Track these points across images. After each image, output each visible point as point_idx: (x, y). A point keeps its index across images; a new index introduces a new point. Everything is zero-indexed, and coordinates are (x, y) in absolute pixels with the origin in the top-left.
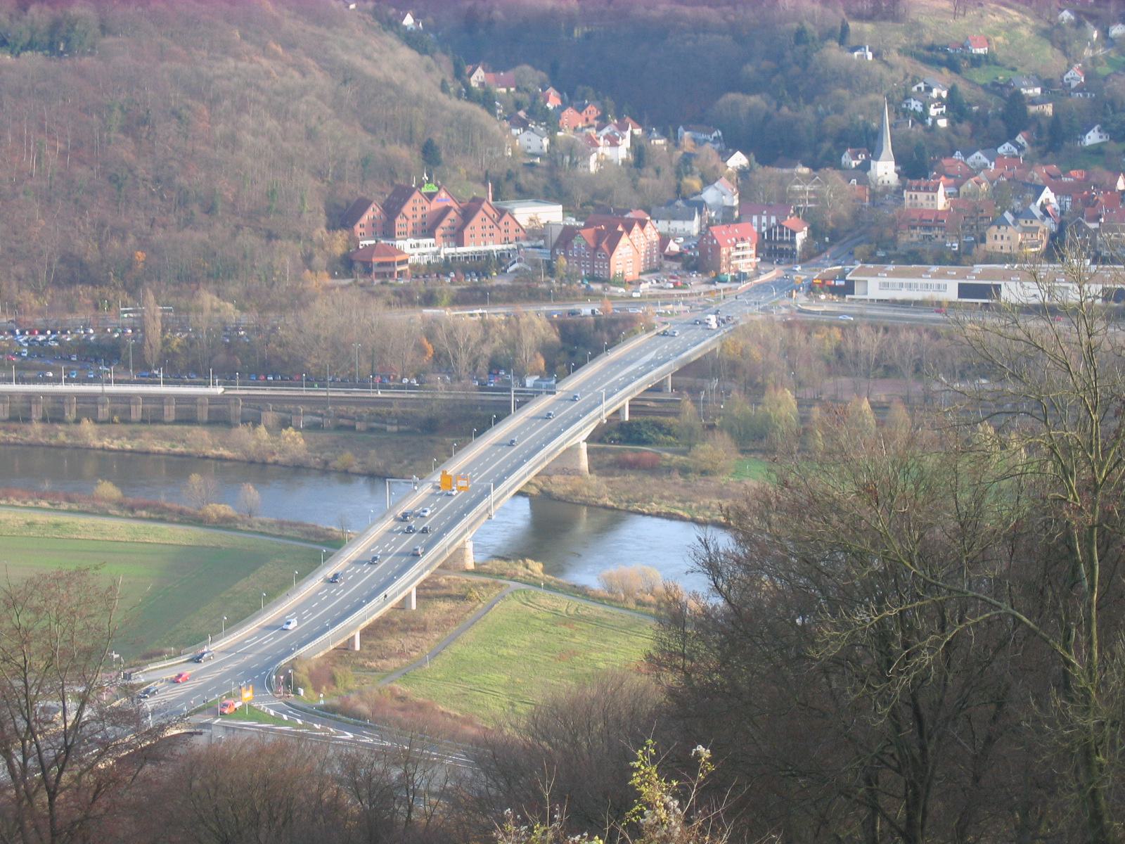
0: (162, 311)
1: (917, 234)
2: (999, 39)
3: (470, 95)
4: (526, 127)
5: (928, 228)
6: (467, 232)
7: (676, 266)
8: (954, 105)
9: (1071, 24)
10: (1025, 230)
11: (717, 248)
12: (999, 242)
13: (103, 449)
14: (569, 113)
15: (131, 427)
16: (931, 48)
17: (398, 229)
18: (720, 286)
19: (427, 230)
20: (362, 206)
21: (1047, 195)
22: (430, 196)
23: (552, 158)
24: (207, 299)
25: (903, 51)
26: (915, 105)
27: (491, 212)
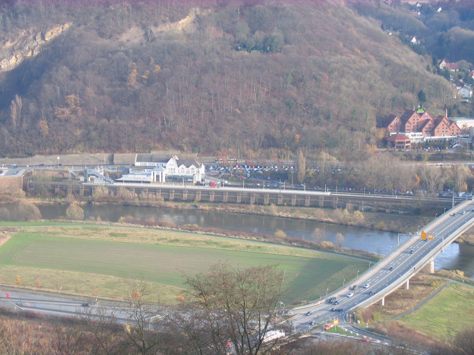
3: (439, 72)
6: (436, 130)
13: (279, 216)
15: (291, 208)
17: (406, 128)
19: (419, 129)
20: (392, 118)
24: (325, 155)
27: (447, 122)
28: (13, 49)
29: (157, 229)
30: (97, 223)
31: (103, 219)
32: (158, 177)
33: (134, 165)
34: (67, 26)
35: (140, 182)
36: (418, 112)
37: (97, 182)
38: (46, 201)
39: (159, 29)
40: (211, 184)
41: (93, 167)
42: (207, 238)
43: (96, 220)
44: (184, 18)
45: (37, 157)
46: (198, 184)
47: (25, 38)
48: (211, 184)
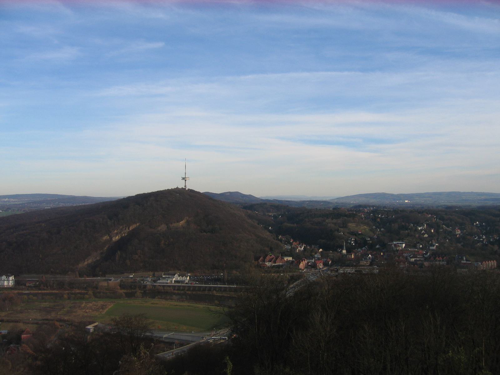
0: (68, 294)
1: (349, 262)
2: (363, 231)
3: (279, 240)
4: (287, 245)
5: (350, 261)
6: (277, 261)
7: (310, 267)
8: (356, 241)
9: (375, 228)
10: (366, 261)
11: (317, 264)
12: (362, 263)
13: (217, 295)
14: (294, 243)
15: (221, 292)
16: (352, 232)
17: (266, 261)
18: (317, 270)
19: (270, 261)
20: (260, 257)
21: (370, 256)
22: (271, 256)
23: (291, 250)
24: (234, 272)
25: (348, 233)
26: (349, 241)
27: (280, 258)
28: (118, 234)
29: (170, 301)
30: (147, 299)
31: (149, 298)
32: (171, 281)
33: (162, 277)
34: (138, 224)
35: (164, 283)
36: (270, 255)
37: (148, 283)
38: (128, 291)
39: (173, 225)
40: (191, 284)
41: (147, 277)
42: (189, 304)
43: (147, 298)
44: (182, 221)
45: (125, 274)
46: (186, 283)
47: (122, 229)
48: (191, 284)
